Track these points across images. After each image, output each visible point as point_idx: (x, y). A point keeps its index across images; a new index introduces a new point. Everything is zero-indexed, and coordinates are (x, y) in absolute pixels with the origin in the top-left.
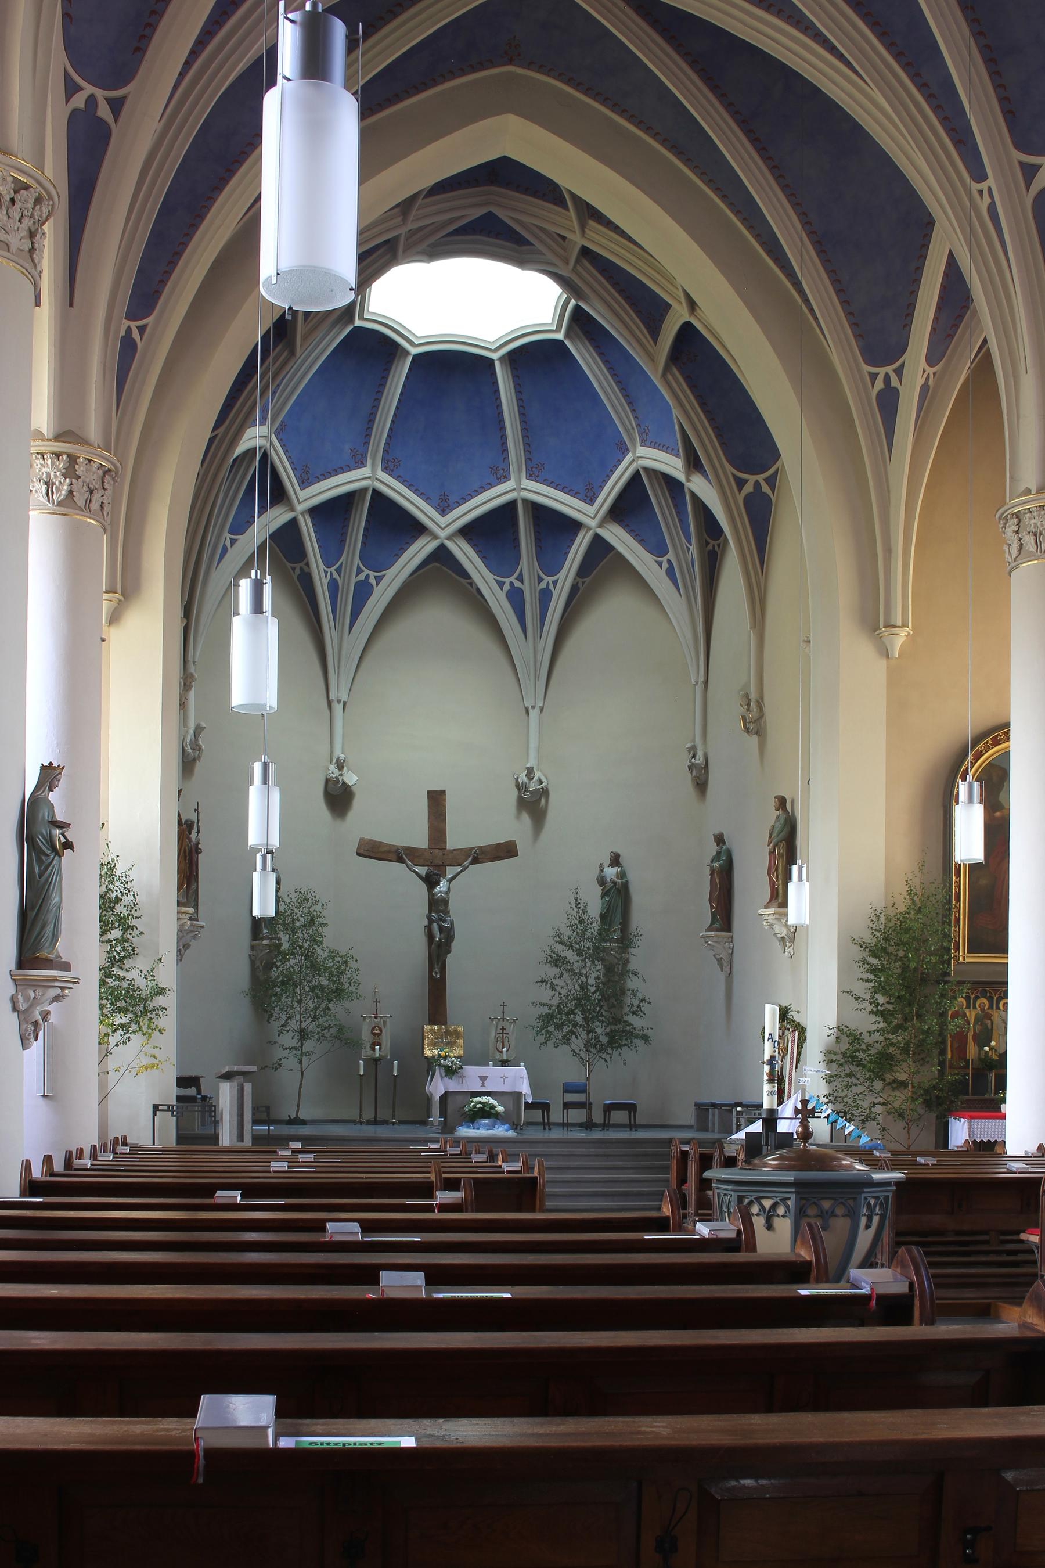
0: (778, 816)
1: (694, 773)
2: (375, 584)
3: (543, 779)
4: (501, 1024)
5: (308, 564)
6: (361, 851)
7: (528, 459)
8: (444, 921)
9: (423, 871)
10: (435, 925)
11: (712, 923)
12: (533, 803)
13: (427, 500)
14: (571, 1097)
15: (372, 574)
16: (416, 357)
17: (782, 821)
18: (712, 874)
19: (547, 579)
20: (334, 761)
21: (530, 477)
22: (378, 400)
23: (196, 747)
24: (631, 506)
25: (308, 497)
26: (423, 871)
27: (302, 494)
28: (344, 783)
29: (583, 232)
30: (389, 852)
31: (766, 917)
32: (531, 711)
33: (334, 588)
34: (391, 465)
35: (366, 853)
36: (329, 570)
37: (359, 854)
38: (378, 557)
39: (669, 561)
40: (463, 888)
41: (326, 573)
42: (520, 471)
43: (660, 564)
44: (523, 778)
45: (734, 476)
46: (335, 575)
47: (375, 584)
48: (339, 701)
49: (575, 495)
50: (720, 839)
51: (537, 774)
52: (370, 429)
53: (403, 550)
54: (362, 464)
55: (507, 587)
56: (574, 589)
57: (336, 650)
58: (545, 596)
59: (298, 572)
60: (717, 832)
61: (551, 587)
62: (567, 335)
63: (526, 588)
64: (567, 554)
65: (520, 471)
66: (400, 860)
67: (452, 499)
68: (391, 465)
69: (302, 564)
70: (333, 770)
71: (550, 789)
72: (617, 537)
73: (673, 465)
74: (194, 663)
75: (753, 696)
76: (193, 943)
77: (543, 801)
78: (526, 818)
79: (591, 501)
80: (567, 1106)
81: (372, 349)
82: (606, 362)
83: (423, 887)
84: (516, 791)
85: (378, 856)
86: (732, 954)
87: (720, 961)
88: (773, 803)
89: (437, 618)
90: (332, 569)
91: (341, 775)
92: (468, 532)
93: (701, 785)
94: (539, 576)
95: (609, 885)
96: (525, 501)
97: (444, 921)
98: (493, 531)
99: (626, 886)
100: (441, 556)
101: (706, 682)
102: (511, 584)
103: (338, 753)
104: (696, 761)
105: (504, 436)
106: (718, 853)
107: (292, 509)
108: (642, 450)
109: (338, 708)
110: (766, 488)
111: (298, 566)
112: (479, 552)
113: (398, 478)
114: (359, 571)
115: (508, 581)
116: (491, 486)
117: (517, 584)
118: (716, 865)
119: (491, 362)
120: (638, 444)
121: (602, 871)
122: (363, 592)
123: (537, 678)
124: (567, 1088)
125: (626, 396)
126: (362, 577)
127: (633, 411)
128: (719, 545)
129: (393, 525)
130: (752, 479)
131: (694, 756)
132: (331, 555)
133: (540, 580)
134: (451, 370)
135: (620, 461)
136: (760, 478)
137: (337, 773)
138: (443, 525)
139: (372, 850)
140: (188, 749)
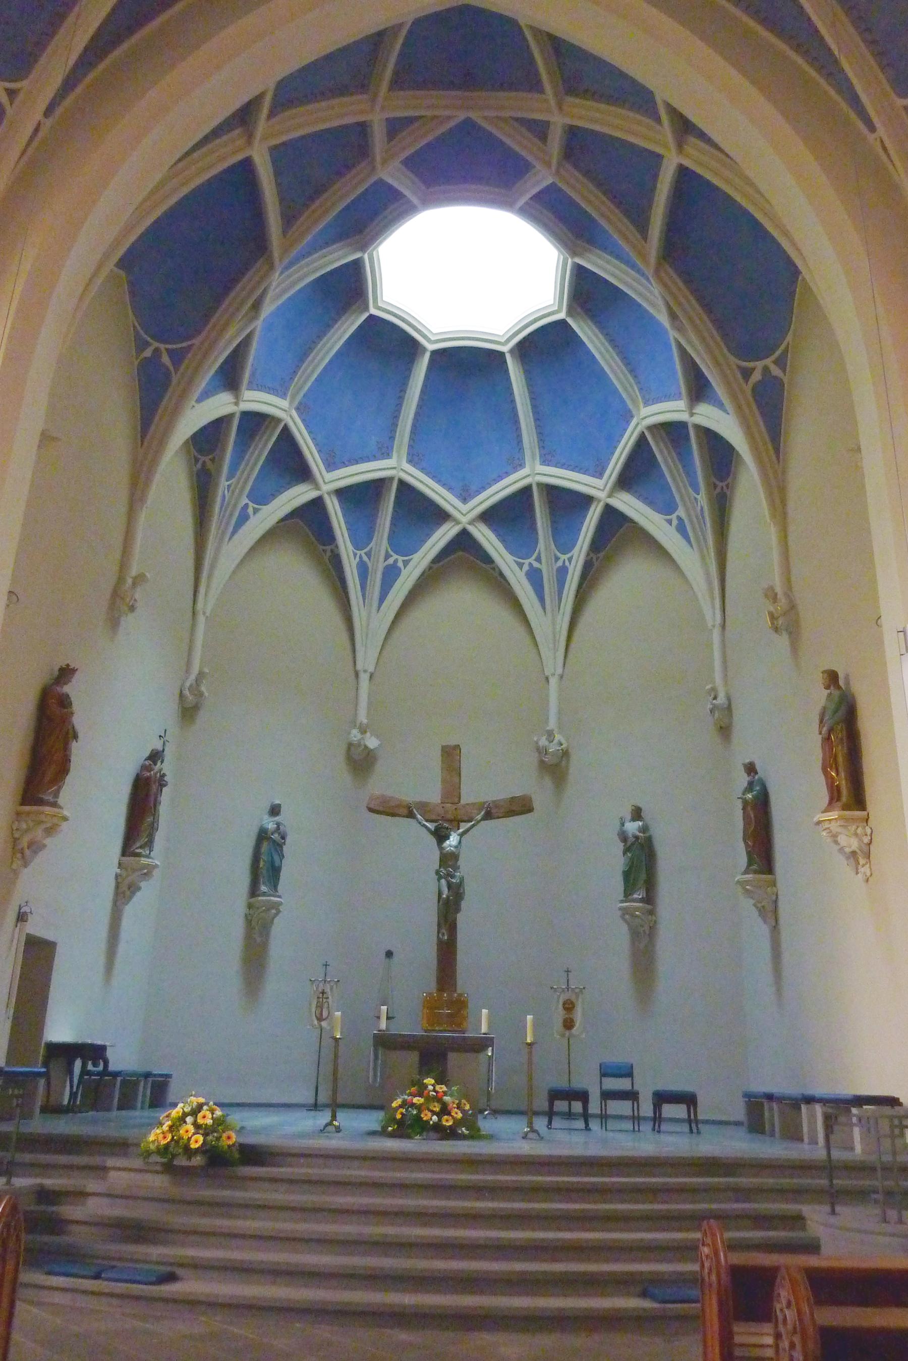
0: (830, 695)
1: (717, 715)
2: (402, 568)
3: (563, 741)
5: (337, 547)
6: (372, 806)
7: (542, 447)
8: (453, 877)
9: (431, 826)
10: (443, 881)
11: (750, 863)
12: (555, 768)
13: (450, 489)
14: (613, 1084)
15: (400, 559)
16: (434, 353)
17: (836, 699)
18: (744, 809)
19: (564, 557)
20: (358, 725)
21: (545, 462)
22: (403, 391)
23: (196, 689)
24: (638, 472)
25: (330, 480)
27: (328, 476)
28: (366, 747)
29: (560, 108)
30: (398, 806)
31: (826, 825)
33: (363, 571)
34: (416, 459)
36: (358, 552)
37: (371, 810)
38: (403, 544)
39: (679, 519)
41: (355, 555)
42: (533, 458)
43: (670, 522)
44: (543, 742)
45: (739, 367)
46: (365, 558)
47: (402, 568)
48: (365, 671)
49: (585, 472)
50: (751, 769)
51: (558, 737)
52: (395, 425)
53: (429, 536)
54: (387, 455)
55: (526, 568)
56: (588, 566)
57: (364, 623)
58: (562, 572)
59: (329, 554)
60: (747, 761)
61: (567, 563)
62: (570, 312)
63: (544, 568)
64: (580, 530)
65: (533, 458)
66: (411, 815)
67: (473, 488)
68: (416, 459)
69: (332, 547)
72: (629, 504)
73: (673, 409)
74: (204, 613)
75: (779, 590)
78: (548, 782)
79: (600, 475)
80: (607, 1095)
81: (390, 343)
82: (607, 335)
83: (433, 841)
84: (537, 755)
86: (776, 902)
87: (762, 911)
88: (819, 679)
89: (463, 599)
90: (362, 552)
91: (363, 738)
92: (488, 517)
93: (725, 731)
94: (555, 555)
95: (631, 840)
96: (539, 485)
97: (453, 877)
98: (510, 515)
99: (649, 840)
100: (464, 542)
101: (723, 626)
102: (530, 564)
105: (518, 429)
106: (751, 785)
107: (317, 487)
108: (645, 411)
110: (776, 371)
111: (328, 548)
112: (498, 536)
113: (422, 470)
114: (387, 556)
115: (527, 562)
116: (507, 474)
117: (536, 565)
118: (750, 796)
119: (501, 355)
120: (641, 405)
121: (623, 825)
122: (391, 574)
123: (555, 650)
124: (606, 1072)
125: (627, 364)
126: (391, 561)
127: (635, 377)
128: (727, 486)
129: (418, 512)
130: (759, 365)
131: (715, 698)
132: (361, 539)
133: (557, 559)
134: (466, 366)
135: (625, 430)
136: (768, 362)
137: (359, 736)
138: (464, 512)
139: (388, 808)
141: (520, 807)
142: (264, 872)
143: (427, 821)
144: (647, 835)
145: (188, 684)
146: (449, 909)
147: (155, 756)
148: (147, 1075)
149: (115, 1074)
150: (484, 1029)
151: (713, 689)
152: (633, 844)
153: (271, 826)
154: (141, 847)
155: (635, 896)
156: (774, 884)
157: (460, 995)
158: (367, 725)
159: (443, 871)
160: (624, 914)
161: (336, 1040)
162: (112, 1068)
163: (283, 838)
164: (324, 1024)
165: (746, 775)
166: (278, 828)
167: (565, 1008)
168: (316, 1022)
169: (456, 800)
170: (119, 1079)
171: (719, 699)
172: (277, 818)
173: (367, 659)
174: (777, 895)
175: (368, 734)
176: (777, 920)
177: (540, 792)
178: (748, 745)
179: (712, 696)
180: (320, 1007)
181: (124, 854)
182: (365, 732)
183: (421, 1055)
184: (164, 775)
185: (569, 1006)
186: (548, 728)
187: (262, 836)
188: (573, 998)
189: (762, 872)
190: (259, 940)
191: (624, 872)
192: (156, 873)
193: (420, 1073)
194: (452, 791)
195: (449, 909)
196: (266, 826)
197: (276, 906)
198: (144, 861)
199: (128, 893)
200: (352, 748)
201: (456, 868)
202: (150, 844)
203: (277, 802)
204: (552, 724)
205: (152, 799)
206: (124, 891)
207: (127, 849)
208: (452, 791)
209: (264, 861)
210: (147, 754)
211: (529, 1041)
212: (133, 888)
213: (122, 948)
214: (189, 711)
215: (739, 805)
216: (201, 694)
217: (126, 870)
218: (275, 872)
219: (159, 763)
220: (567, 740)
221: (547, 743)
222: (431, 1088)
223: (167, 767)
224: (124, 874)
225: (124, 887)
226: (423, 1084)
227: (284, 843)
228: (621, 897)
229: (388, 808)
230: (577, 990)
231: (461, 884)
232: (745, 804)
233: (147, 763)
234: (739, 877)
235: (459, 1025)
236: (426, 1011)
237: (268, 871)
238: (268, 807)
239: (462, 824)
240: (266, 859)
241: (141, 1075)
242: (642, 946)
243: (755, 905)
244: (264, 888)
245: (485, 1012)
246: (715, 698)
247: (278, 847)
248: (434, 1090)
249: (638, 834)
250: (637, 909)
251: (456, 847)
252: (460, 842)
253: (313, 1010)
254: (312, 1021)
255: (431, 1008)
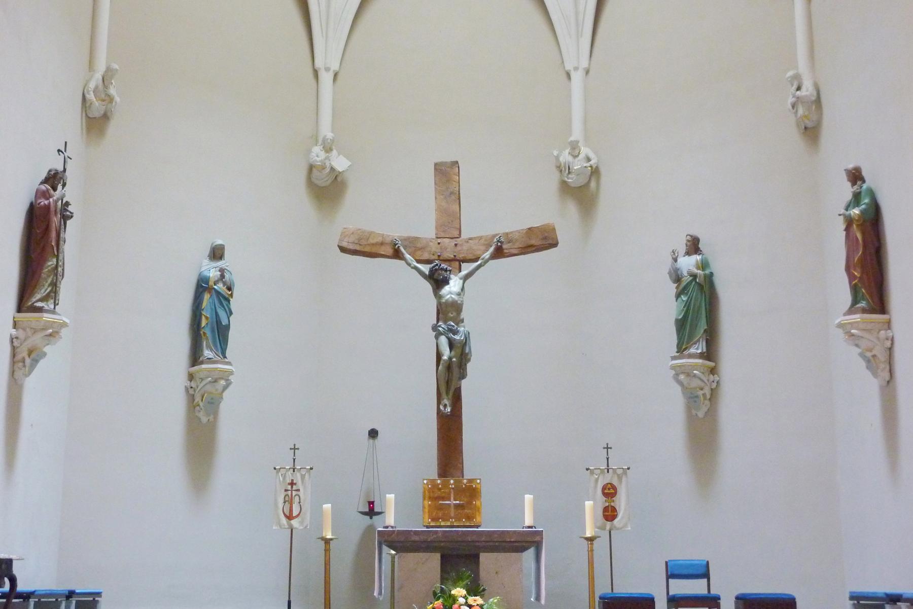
1: (801, 111)
4: (608, 478)
6: (345, 244)
8: (455, 332)
9: (425, 268)
10: (443, 340)
11: (855, 301)
12: (581, 192)
14: (682, 588)
18: (848, 229)
20: (320, 142)
26: (425, 268)
30: (382, 244)
32: (573, 74)
35: (351, 247)
37: (343, 250)
40: (482, 293)
44: (565, 157)
48: (327, 69)
50: (856, 176)
51: (584, 151)
66: (397, 254)
70: (318, 154)
71: (603, 170)
76: (188, 384)
77: (593, 184)
78: (572, 209)
83: (427, 287)
84: (557, 174)
85: (367, 249)
86: (891, 349)
87: (871, 363)
91: (327, 158)
93: (811, 132)
95: (686, 279)
97: (455, 332)
99: (710, 278)
103: (326, 131)
104: (803, 93)
106: (857, 198)
109: (326, 78)
118: (856, 211)
121: (675, 260)
123: (579, 35)
131: (799, 89)
137: (323, 155)
139: (363, 248)
140: (91, 96)
141: (541, 241)
142: (209, 334)
143: (419, 261)
144: (707, 272)
145: (92, 85)
146: (452, 373)
147: (54, 179)
148: (70, 595)
149: (26, 596)
150: (528, 521)
151: (797, 77)
152: (691, 282)
153: (213, 274)
154: (41, 300)
155: (692, 350)
156: (888, 325)
157: (470, 481)
158: (333, 141)
159: (442, 326)
160: (677, 375)
161: (327, 541)
162: (21, 587)
163: (229, 289)
164: (295, 523)
165: (849, 184)
166: (222, 276)
167: (604, 494)
168: (284, 520)
169: (456, 234)
170: (32, 602)
171: (804, 88)
172: (220, 264)
173: (329, 54)
174: (892, 340)
175: (335, 152)
176: (891, 372)
177: (564, 219)
178: (843, 147)
179: (795, 87)
180: (289, 500)
181: (19, 309)
182: (331, 150)
183: (442, 557)
184: (67, 204)
185: (610, 492)
186: (572, 139)
187: (202, 286)
188: (615, 483)
189: (871, 311)
190: (204, 420)
191: (677, 321)
192: (64, 332)
193: (443, 580)
194: (449, 221)
195: (452, 373)
196: (206, 274)
197: (226, 376)
198: (47, 317)
199: (28, 361)
200: (314, 170)
201: (459, 321)
202: (53, 294)
203: (219, 242)
204: (577, 134)
205: (53, 234)
206: (23, 358)
207: (24, 301)
208: (449, 221)
209: (207, 318)
210: (43, 175)
211: (588, 535)
212: (35, 355)
213: (25, 433)
214: (96, 123)
215: (841, 225)
216: (111, 99)
217: (24, 329)
218: (222, 332)
219: (60, 187)
220: (596, 153)
221: (570, 159)
222: (462, 601)
223: (70, 192)
224: (21, 334)
225: (23, 353)
226: (450, 596)
227: (231, 295)
228: (673, 351)
229: (363, 248)
230: (620, 472)
231: (465, 343)
232: (849, 222)
233: (43, 187)
234: (841, 319)
235: (469, 518)
236: (427, 503)
237: (213, 331)
238: (207, 251)
239: (463, 265)
240: (209, 320)
241: (60, 595)
242: (701, 414)
243: (862, 355)
244: (207, 353)
245: (528, 498)
246: (799, 89)
247: (224, 300)
248: (467, 604)
249: (696, 271)
250: (695, 367)
251: (459, 294)
252: (463, 289)
253: (281, 505)
254: (279, 520)
255: (434, 499)
